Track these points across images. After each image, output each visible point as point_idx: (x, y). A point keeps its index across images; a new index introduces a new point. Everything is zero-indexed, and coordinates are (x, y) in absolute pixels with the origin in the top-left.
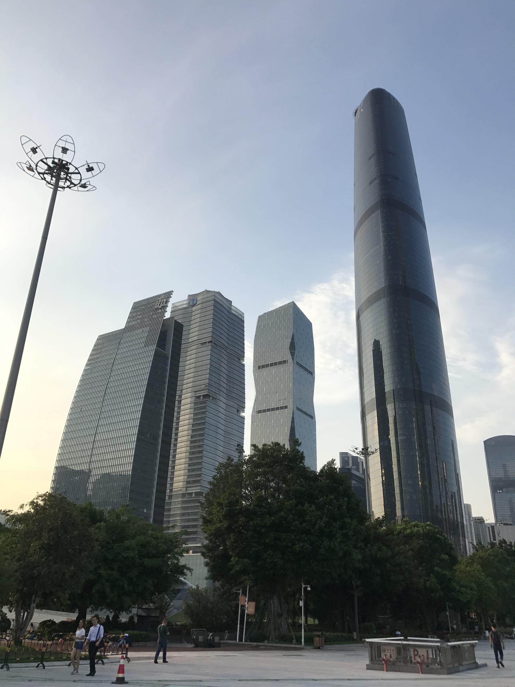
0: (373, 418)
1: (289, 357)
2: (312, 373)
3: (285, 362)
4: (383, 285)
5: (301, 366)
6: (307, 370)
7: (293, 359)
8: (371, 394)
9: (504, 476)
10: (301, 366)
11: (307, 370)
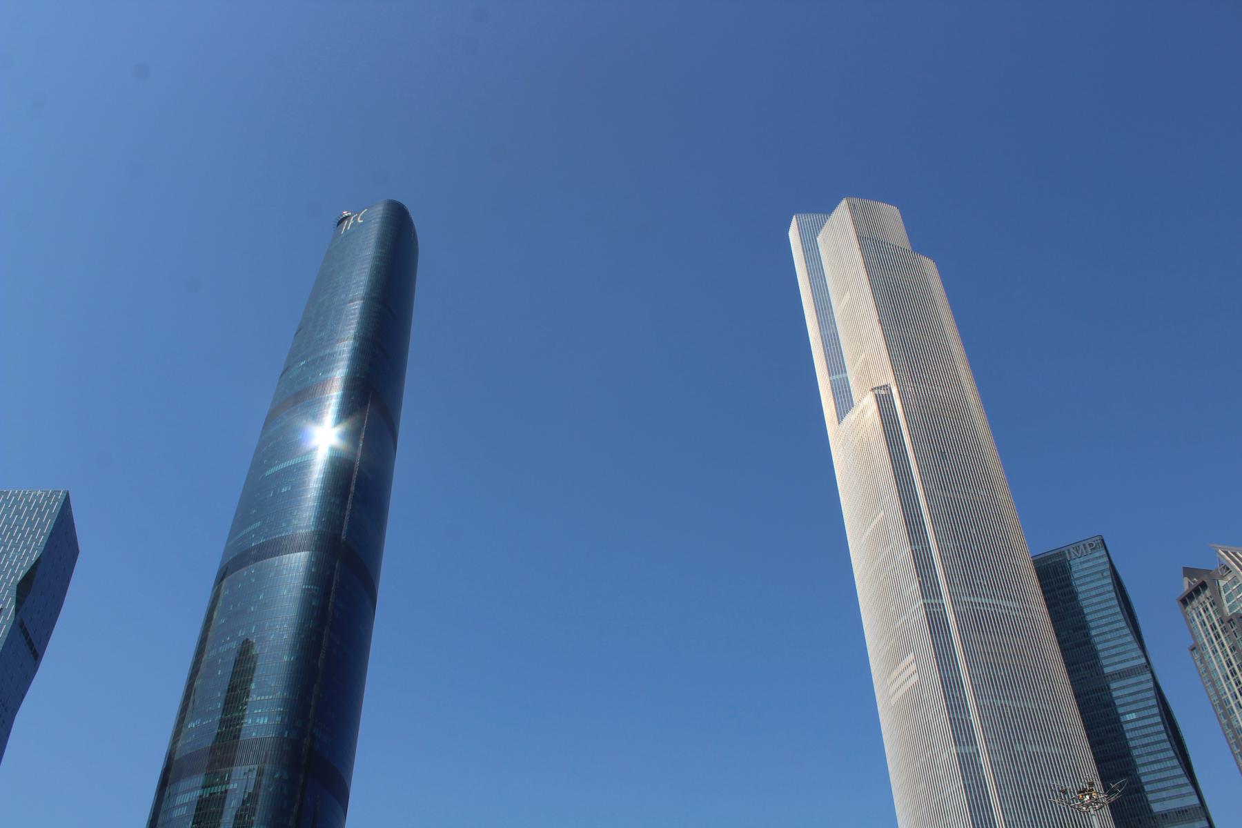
5: (25, 633)
7: (17, 610)
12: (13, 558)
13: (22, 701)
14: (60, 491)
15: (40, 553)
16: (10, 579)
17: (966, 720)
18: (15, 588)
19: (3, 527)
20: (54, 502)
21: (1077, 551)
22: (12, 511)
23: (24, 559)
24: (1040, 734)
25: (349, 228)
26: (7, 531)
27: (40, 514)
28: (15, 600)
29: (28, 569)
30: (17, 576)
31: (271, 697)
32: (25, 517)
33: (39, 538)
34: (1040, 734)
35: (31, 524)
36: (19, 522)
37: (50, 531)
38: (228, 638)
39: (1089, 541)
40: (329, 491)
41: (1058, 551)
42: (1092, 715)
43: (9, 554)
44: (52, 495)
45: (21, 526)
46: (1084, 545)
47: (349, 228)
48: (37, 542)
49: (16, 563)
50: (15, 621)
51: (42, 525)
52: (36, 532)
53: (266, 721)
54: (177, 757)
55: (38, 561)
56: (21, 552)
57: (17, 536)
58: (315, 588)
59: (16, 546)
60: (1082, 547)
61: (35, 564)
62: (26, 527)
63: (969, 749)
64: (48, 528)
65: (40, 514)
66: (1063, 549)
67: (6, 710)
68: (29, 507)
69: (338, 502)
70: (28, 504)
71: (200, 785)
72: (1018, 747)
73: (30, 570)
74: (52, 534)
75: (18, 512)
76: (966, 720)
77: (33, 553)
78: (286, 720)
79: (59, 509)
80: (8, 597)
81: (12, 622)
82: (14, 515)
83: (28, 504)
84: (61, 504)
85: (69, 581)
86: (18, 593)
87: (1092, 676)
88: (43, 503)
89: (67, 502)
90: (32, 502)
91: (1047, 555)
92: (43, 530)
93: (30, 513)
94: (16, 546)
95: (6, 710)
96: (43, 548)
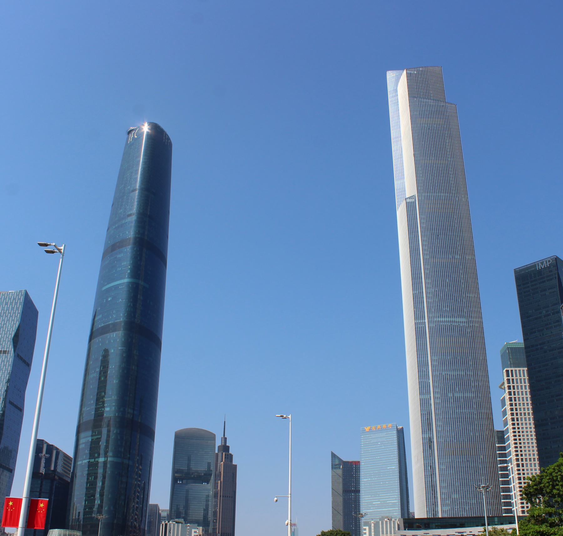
1: (11, 349)
2: (29, 364)
3: (5, 352)
5: (21, 358)
6: (24, 361)
7: (15, 351)
8: (90, 415)
9: (186, 469)
10: (21, 358)
11: (24, 361)
12: (8, 326)
13: (27, 385)
14: (22, 291)
15: (19, 322)
16: (9, 336)
17: (427, 382)
18: (12, 341)
19: (1, 312)
20: (21, 296)
21: (542, 265)
22: (4, 303)
23: (13, 326)
24: (463, 387)
25: (131, 140)
26: (3, 314)
27: (16, 303)
28: (13, 346)
29: (16, 331)
30: (12, 335)
31: (110, 399)
32: (10, 305)
33: (17, 315)
34: (463, 387)
35: (13, 308)
36: (8, 309)
37: (21, 312)
38: (93, 372)
39: (549, 259)
40: (127, 300)
41: (534, 264)
42: (537, 357)
43: (6, 325)
44: (19, 293)
45: (9, 310)
46: (546, 261)
47: (131, 140)
48: (17, 317)
49: (10, 328)
50: (15, 356)
51: (18, 309)
52: (15, 312)
53: (109, 409)
54: (81, 422)
55: (19, 326)
56: (11, 323)
57: (8, 315)
58: (124, 348)
59: (8, 320)
60: (545, 262)
61: (18, 328)
62: (11, 311)
63: (426, 397)
64: (20, 310)
65: (16, 303)
66: (535, 263)
67: (20, 392)
68: (11, 300)
69: (132, 305)
70: (10, 299)
71: (90, 435)
72: (450, 395)
73: (16, 331)
74: (23, 312)
75: (7, 304)
76: (427, 382)
77: (16, 323)
78: (116, 408)
79: (24, 299)
80: (10, 345)
81: (13, 356)
82: (5, 305)
83: (10, 299)
84: (24, 297)
85: (36, 327)
86: (14, 343)
87: (540, 335)
88: (16, 298)
89: (27, 295)
90: (11, 298)
91: (528, 266)
92: (18, 311)
93: (11, 303)
94: (8, 320)
95: (20, 392)
96: (20, 320)
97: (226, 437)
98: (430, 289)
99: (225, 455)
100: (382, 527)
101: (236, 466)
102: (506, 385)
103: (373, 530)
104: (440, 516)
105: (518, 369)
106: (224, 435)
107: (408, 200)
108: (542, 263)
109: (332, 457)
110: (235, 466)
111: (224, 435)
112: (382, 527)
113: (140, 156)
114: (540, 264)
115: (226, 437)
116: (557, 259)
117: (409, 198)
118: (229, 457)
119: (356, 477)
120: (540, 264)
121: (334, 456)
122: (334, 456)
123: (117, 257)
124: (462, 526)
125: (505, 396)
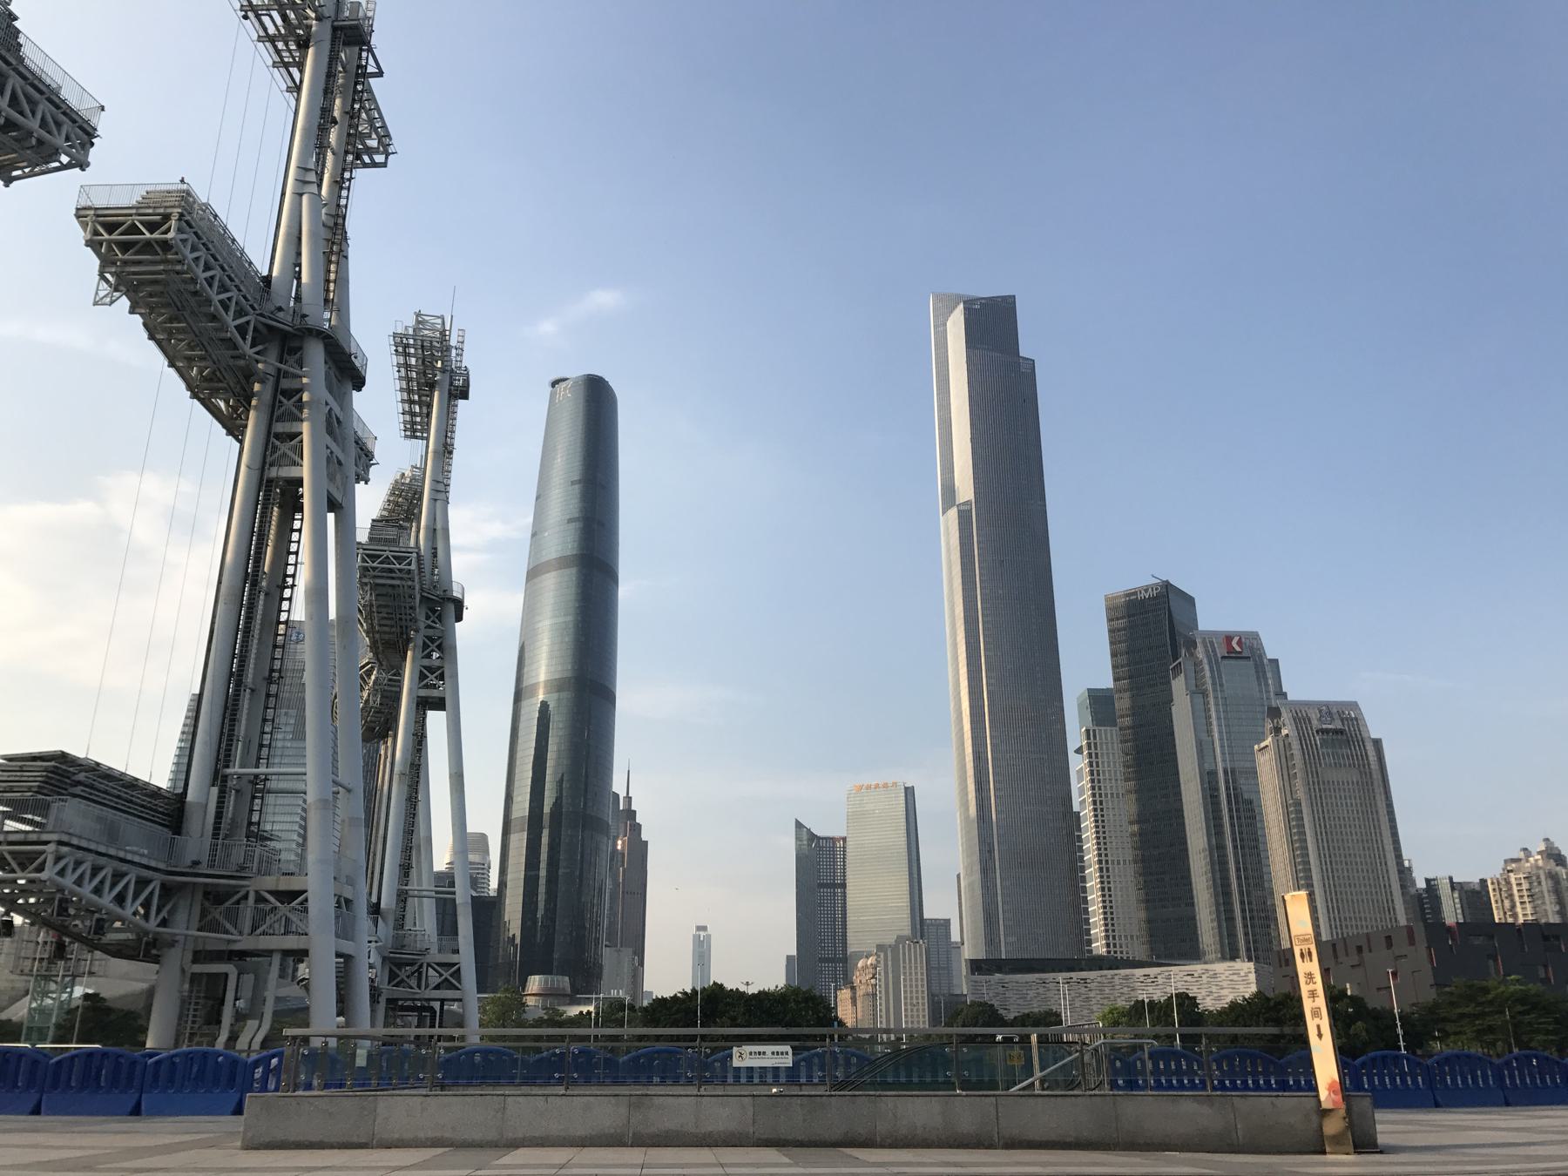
0: (519, 841)
4: (569, 674)
60: (1150, 590)
97: (630, 795)
98: (1322, 761)
99: (630, 825)
100: (904, 954)
101: (635, 812)
102: (1085, 753)
103: (890, 958)
104: (1004, 957)
105: (1102, 728)
106: (628, 793)
107: (962, 508)
108: (1146, 591)
109: (796, 827)
110: (646, 843)
111: (628, 793)
112: (904, 954)
113: (978, 542)
114: (1143, 592)
115: (630, 795)
116: (1167, 586)
117: (964, 504)
118: (637, 828)
119: (406, 355)
120: (1143, 592)
121: (799, 825)
122: (799, 825)
123: (565, 1012)
124: (1043, 971)
125: (144, 234)
